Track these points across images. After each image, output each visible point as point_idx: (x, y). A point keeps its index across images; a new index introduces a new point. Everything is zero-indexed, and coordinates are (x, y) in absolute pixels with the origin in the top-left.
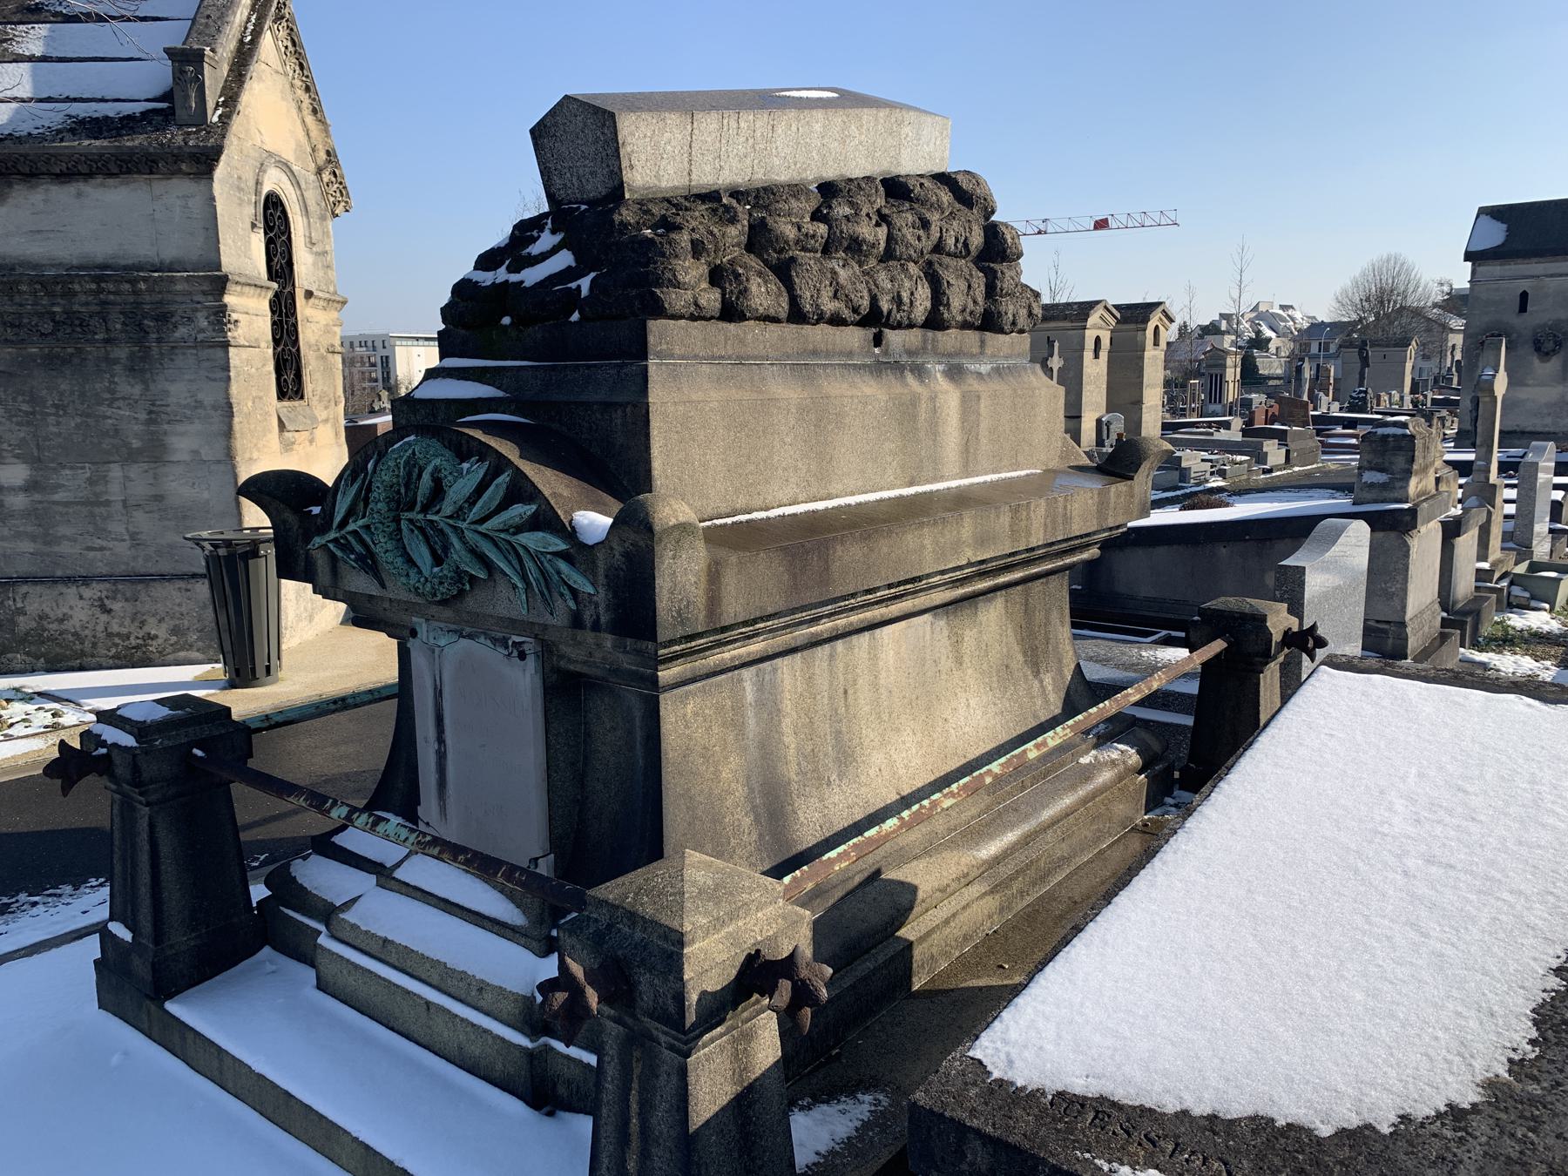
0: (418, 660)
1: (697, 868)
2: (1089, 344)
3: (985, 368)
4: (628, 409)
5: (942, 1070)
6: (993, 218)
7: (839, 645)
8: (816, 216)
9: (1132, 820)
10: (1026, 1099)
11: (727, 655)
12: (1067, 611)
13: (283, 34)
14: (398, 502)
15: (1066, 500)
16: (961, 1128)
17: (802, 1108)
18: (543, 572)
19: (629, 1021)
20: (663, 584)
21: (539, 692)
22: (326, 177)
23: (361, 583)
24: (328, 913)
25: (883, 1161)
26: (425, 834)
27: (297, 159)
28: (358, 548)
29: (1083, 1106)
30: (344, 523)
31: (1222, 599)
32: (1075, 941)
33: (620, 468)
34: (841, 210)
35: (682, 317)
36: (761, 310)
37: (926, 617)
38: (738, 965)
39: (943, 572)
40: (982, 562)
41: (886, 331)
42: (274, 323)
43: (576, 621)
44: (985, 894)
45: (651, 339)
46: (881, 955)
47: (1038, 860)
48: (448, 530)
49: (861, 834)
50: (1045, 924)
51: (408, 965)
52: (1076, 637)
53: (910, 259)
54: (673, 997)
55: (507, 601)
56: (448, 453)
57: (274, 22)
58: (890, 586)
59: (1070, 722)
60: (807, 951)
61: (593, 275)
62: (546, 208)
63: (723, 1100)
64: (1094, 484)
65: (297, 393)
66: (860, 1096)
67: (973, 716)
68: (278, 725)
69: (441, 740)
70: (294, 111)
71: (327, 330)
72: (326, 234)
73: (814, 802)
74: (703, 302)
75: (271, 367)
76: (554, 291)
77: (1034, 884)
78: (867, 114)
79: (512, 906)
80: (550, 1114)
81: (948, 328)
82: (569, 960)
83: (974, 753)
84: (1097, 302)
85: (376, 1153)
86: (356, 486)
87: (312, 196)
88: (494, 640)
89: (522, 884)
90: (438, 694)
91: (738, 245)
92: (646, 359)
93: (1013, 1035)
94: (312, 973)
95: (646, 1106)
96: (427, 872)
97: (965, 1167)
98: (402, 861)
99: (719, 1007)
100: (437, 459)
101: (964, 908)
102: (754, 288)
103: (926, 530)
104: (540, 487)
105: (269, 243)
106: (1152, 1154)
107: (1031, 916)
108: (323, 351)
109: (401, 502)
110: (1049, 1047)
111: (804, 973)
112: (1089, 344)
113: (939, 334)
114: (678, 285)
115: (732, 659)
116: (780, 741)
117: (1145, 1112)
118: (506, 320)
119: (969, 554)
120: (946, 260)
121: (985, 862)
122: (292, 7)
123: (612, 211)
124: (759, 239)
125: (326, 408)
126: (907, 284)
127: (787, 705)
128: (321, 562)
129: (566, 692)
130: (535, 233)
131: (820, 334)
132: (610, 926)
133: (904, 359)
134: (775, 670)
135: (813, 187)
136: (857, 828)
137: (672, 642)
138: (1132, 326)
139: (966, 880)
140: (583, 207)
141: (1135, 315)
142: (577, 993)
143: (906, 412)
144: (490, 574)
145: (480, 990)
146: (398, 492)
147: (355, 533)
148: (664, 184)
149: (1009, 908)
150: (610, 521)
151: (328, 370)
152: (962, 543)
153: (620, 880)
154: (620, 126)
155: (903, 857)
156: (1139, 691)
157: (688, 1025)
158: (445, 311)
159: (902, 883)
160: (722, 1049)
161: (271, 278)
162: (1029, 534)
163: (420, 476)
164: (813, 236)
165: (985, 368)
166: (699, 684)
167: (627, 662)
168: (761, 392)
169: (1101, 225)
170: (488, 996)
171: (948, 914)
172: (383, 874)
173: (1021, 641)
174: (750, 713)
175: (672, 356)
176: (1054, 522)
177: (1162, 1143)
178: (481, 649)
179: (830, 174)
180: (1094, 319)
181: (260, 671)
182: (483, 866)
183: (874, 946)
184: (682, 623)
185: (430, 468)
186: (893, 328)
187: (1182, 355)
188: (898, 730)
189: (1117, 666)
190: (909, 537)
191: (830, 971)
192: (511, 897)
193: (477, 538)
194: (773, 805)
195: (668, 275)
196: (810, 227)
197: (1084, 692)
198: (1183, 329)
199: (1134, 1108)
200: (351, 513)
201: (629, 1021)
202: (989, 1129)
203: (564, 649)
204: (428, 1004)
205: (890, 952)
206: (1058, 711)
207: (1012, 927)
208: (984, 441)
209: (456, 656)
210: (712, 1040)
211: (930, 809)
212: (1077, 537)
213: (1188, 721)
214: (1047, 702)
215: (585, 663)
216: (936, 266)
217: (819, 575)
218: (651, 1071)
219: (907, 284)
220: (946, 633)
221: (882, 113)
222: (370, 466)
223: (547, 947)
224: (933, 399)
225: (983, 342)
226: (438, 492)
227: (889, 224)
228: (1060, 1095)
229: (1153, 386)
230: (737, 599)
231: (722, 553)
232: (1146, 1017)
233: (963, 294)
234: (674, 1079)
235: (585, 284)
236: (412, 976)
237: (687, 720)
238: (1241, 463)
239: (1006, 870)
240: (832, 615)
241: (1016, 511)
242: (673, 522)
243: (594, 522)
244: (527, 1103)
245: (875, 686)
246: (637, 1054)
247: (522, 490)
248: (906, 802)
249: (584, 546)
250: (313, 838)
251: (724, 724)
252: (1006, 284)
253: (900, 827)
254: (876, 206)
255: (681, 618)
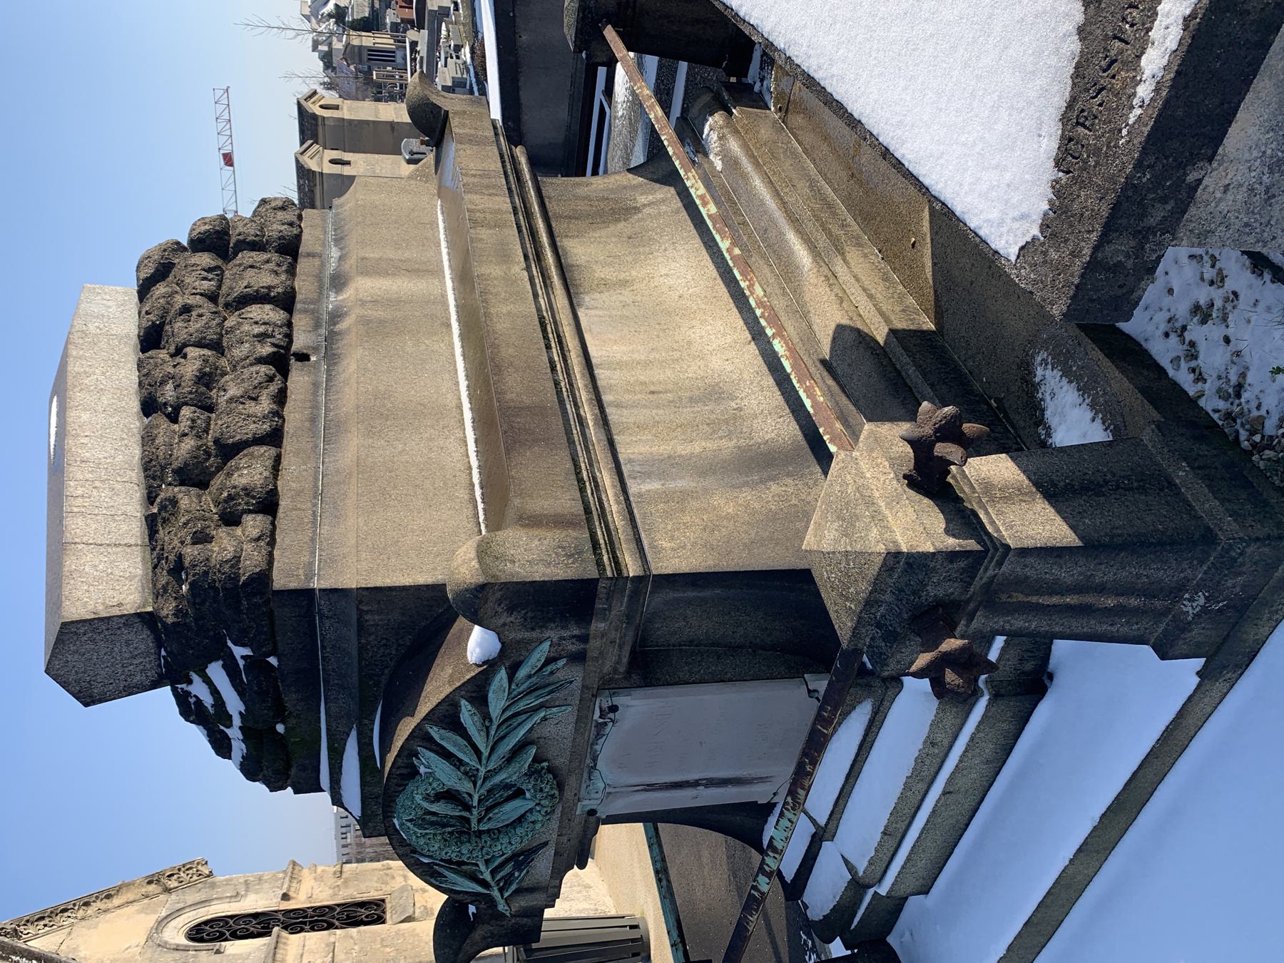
0: (619, 807)
1: (821, 539)
2: (337, 169)
3: (335, 253)
4: (365, 608)
5: (1030, 288)
6: (185, 243)
7: (607, 398)
8: (174, 418)
9: (775, 122)
10: (1062, 200)
11: (614, 508)
12: (577, 179)
13: (31, 929)
14: (461, 833)
15: (466, 175)
16: (1093, 266)
17: (1049, 435)
18: (529, 692)
19: (972, 605)
20: (540, 573)
21: (649, 691)
22: (173, 883)
23: (542, 865)
24: (857, 886)
25: (1101, 356)
26: (786, 803)
27: (155, 912)
28: (508, 869)
29: (1070, 140)
30: (484, 883)
31: (566, 30)
32: (897, 155)
33: (421, 619)
34: (168, 393)
35: (271, 554)
36: (266, 474)
37: (581, 313)
38: (919, 497)
39: (535, 296)
40: (526, 257)
41: (294, 348)
42: (313, 929)
43: (578, 658)
44: (844, 260)
45: (293, 585)
46: (902, 359)
47: (812, 210)
48: (488, 785)
49: (788, 375)
50: (875, 190)
51: (908, 812)
52: (606, 172)
53: (221, 325)
54: (951, 562)
55: (558, 726)
56: (410, 787)
57: (19, 938)
58: (548, 347)
59: (682, 172)
60: (905, 428)
61: (230, 644)
62: (167, 690)
63: (1050, 511)
64: (452, 149)
65: (378, 905)
66: (1037, 380)
67: (678, 270)
68: (681, 935)
69: (696, 784)
70: (109, 916)
71: (319, 879)
72: (228, 882)
73: (757, 424)
74: (255, 533)
75: (353, 931)
76: (253, 682)
77: (834, 214)
78: (74, 368)
79: (853, 714)
80: (1051, 677)
81: (293, 288)
82: (914, 668)
83: (712, 271)
84: (297, 161)
85: (1085, 842)
86: (446, 873)
87: (191, 896)
88: (599, 735)
89: (835, 709)
90: (651, 787)
91: (199, 496)
92: (314, 590)
93: (994, 215)
94: (912, 899)
95: (1055, 588)
96: (820, 799)
97: (1130, 264)
98: (810, 818)
99: (961, 515)
100: (416, 798)
101: (858, 280)
102: (244, 481)
103: (493, 311)
104: (442, 696)
105: (236, 936)
106: (1124, 63)
107: (866, 218)
108: (339, 883)
109: (462, 830)
110: (1008, 176)
111: (928, 430)
112: (337, 169)
113: (299, 297)
114: (237, 558)
115: (618, 503)
116: (699, 456)
117: (1079, 73)
118: (280, 728)
119: (518, 268)
120: (224, 289)
121: (814, 260)
122: (6, 922)
123: (164, 624)
124: (194, 476)
125: (393, 878)
126: (246, 328)
127: (664, 449)
128: (523, 902)
129: (649, 666)
130: (192, 700)
131: (294, 416)
132: (879, 625)
133: (323, 331)
134: (630, 461)
135: (146, 420)
136: (782, 381)
137: (599, 563)
138: (320, 129)
139: (832, 278)
140: (163, 653)
141: (310, 127)
142: (947, 660)
143: (375, 329)
144: (532, 743)
145: (933, 744)
146: (451, 833)
147: (493, 873)
148: (139, 572)
149: (858, 237)
150: (477, 629)
151: (357, 876)
152: (507, 274)
153: (833, 616)
154: (76, 617)
155: (810, 337)
156: (652, 107)
157: (979, 548)
158: (274, 786)
159: (834, 339)
160: (1000, 513)
161: (268, 934)
162: (499, 211)
163: (434, 814)
164: (193, 421)
165: (335, 253)
166: (643, 535)
167: (620, 606)
168: (350, 474)
169: (228, 160)
170: (939, 737)
171: (862, 294)
172: (820, 837)
173: (606, 223)
174: (671, 485)
175: (311, 564)
176: (488, 187)
177: (1113, 53)
178: (607, 749)
179: (134, 405)
180: (313, 165)
181: (635, 934)
182: (815, 746)
183: (894, 365)
184: (580, 553)
185: (425, 805)
186: (291, 342)
187: (351, 85)
188: (689, 343)
189: (632, 140)
190: (498, 327)
191: (925, 404)
192: (845, 715)
193: (494, 757)
194: (759, 463)
195: (226, 568)
196: (184, 424)
197: (657, 167)
198: (329, 86)
199: (1074, 84)
200: (473, 877)
201: (972, 605)
202: (1094, 237)
203: (607, 668)
204: (945, 793)
205: (899, 350)
206: (672, 190)
207: (876, 237)
208: (407, 255)
209: (612, 768)
210: (993, 522)
211: (764, 307)
212: (504, 167)
213: (683, 66)
214: (663, 201)
215: (621, 647)
216: (229, 299)
217: (539, 413)
218: (1021, 583)
219: (246, 328)
220: (597, 295)
221: (73, 352)
222: (426, 861)
223: (895, 682)
224: (363, 303)
225: (309, 255)
226: (449, 796)
227: (185, 345)
228: (1058, 163)
229: (377, 111)
230: (557, 498)
231: (511, 514)
232: (979, 77)
233: (260, 273)
234: (1030, 560)
235: (239, 652)
236: (918, 808)
237: (677, 547)
238: (448, 31)
239: (822, 241)
240: (576, 405)
241: (475, 223)
242: (475, 563)
243: (478, 643)
244: (1041, 699)
245: (647, 364)
246: (1004, 598)
247: (447, 715)
248: (758, 335)
249: (502, 652)
250: (787, 899)
251: (683, 511)
252: (251, 231)
253: (782, 337)
254: (167, 358)
255: (575, 554)
